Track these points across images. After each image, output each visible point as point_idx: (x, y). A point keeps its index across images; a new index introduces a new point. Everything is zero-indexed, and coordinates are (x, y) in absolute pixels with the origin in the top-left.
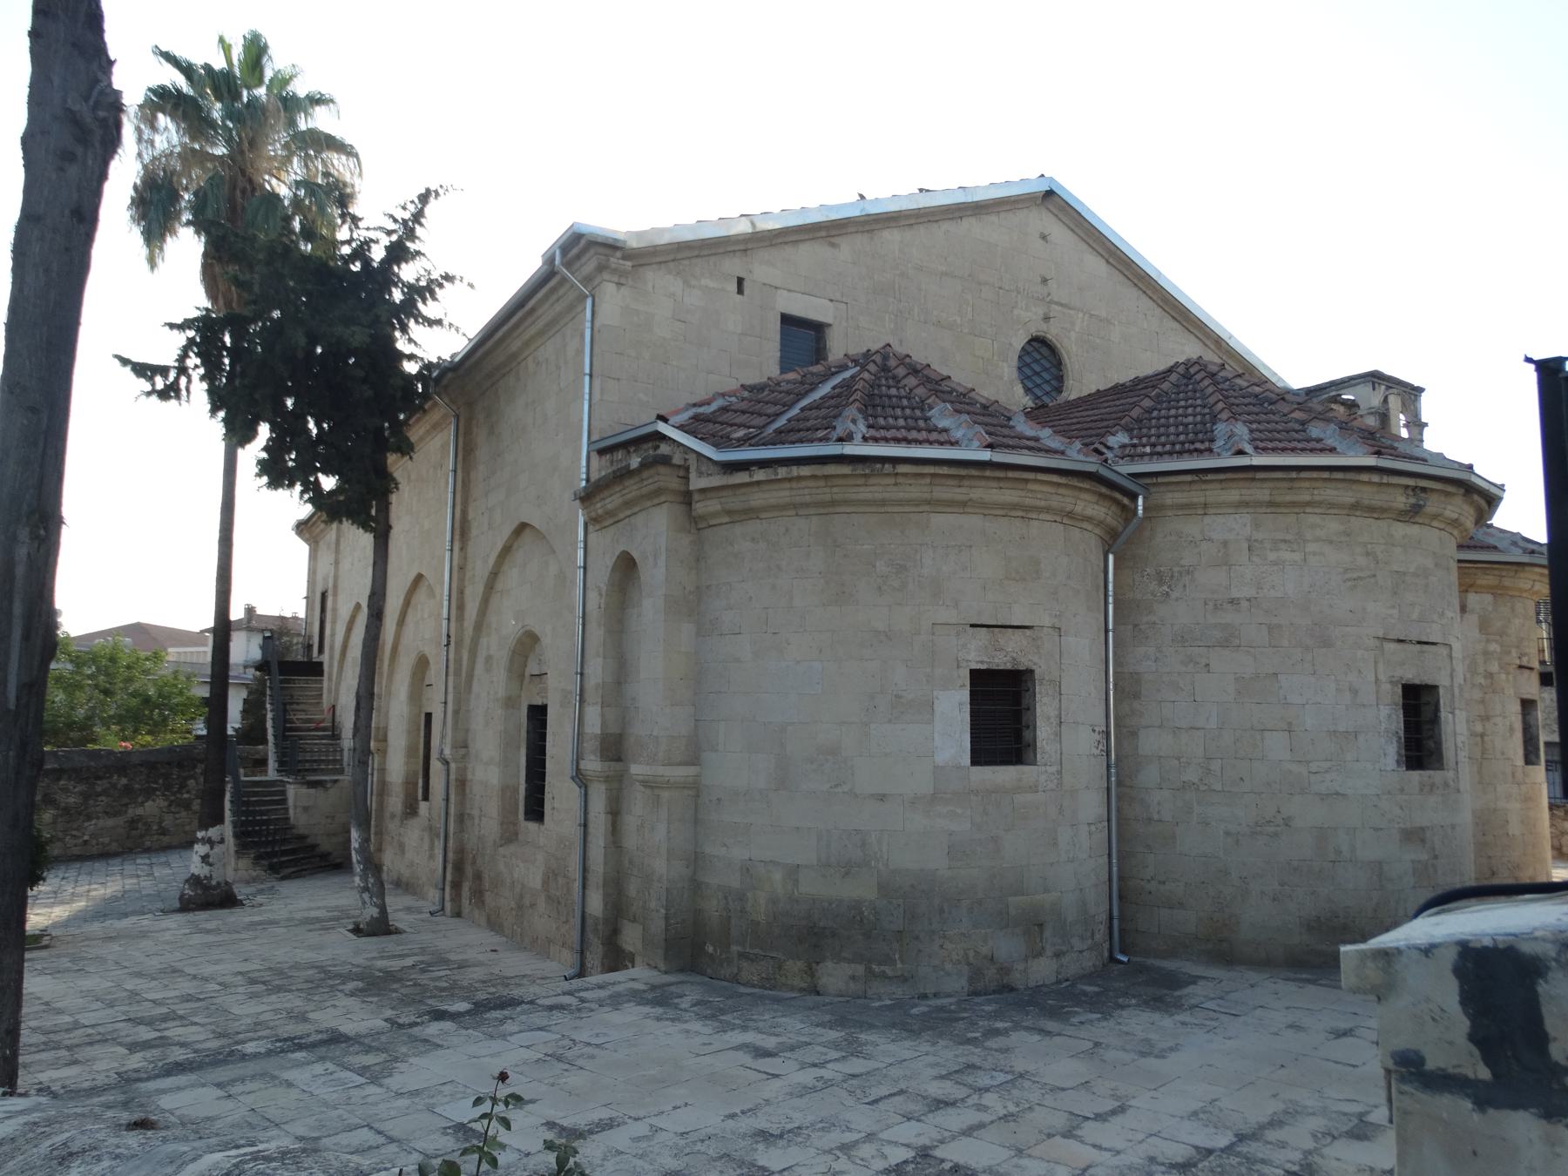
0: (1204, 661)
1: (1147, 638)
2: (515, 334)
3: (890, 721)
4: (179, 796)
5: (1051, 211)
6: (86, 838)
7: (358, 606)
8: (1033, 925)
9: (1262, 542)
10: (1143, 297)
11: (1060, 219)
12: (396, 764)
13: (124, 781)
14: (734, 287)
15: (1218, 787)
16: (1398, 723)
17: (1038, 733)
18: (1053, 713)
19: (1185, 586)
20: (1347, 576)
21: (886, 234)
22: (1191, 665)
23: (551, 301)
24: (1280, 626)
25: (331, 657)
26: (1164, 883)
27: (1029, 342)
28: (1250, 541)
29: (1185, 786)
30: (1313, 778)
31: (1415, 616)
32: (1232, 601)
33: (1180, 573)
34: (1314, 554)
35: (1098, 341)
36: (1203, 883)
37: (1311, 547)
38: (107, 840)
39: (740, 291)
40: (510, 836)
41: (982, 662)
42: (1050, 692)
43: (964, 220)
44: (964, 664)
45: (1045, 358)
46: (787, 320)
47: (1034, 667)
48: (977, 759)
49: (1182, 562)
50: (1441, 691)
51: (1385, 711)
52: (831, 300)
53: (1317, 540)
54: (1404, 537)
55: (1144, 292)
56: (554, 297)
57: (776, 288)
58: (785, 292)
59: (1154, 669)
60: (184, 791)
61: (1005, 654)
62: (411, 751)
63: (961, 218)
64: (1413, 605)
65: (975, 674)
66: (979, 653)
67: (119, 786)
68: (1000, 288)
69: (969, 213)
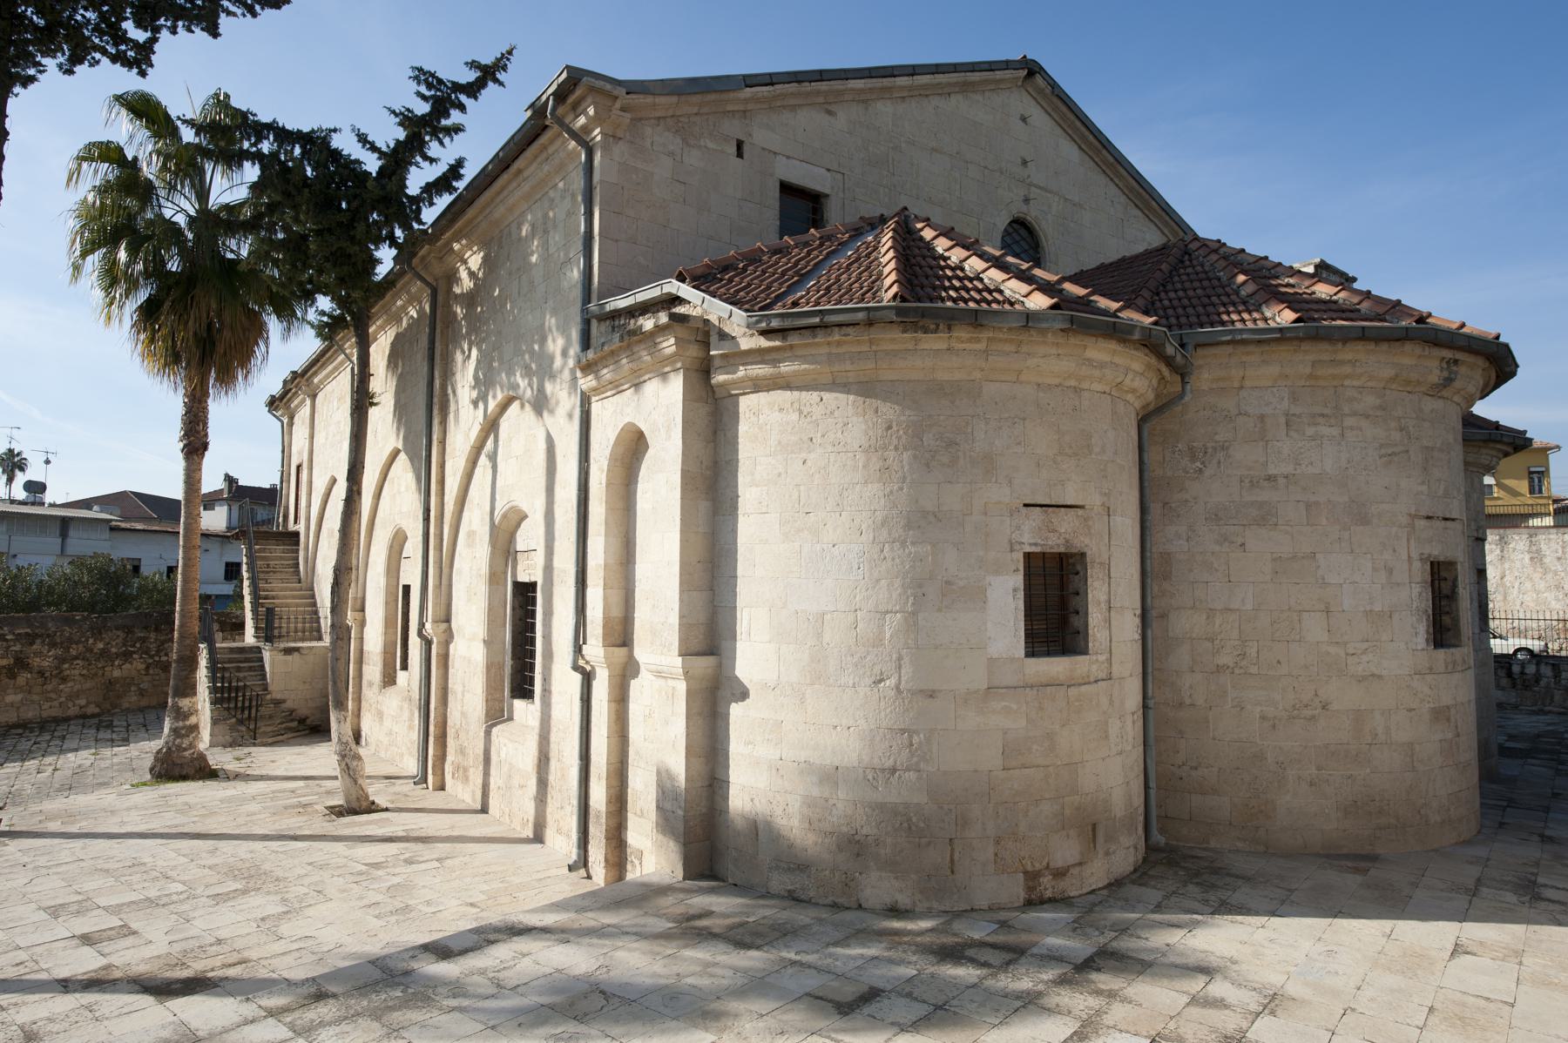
0: (1240, 540)
1: (1179, 516)
2: (498, 200)
3: (940, 610)
4: (157, 658)
5: (1029, 93)
6: (63, 699)
7: (334, 481)
8: (1091, 830)
9: (1299, 416)
10: (1110, 183)
11: (1038, 103)
12: (374, 637)
13: (101, 645)
14: (734, 150)
15: (1254, 670)
16: (1427, 600)
17: (1090, 620)
18: (1103, 598)
19: (1219, 462)
20: (1383, 451)
21: (880, 105)
22: (1227, 544)
23: (539, 160)
24: (1317, 503)
25: (308, 528)
26: (1196, 768)
27: (1012, 222)
28: (1287, 415)
29: (1220, 669)
30: (1350, 659)
31: (1441, 492)
32: (1270, 478)
33: (1215, 449)
34: (1352, 428)
35: (1072, 225)
36: (1238, 769)
37: (1349, 422)
38: (83, 702)
39: (740, 154)
40: (496, 715)
41: (1036, 544)
42: (1101, 577)
43: (952, 95)
44: (1017, 547)
45: (1024, 239)
46: (787, 189)
47: (1085, 550)
48: (1031, 653)
49: (1217, 438)
50: (1459, 567)
51: (1416, 589)
52: (828, 170)
53: (1354, 414)
54: (1432, 411)
55: (1112, 179)
56: (544, 155)
57: (775, 153)
58: (784, 158)
59: (1186, 549)
60: (162, 654)
61: (1059, 535)
62: (389, 622)
63: (949, 94)
64: (1439, 480)
65: (1028, 556)
66: (1032, 535)
67: (95, 651)
68: (986, 167)
69: (957, 90)
